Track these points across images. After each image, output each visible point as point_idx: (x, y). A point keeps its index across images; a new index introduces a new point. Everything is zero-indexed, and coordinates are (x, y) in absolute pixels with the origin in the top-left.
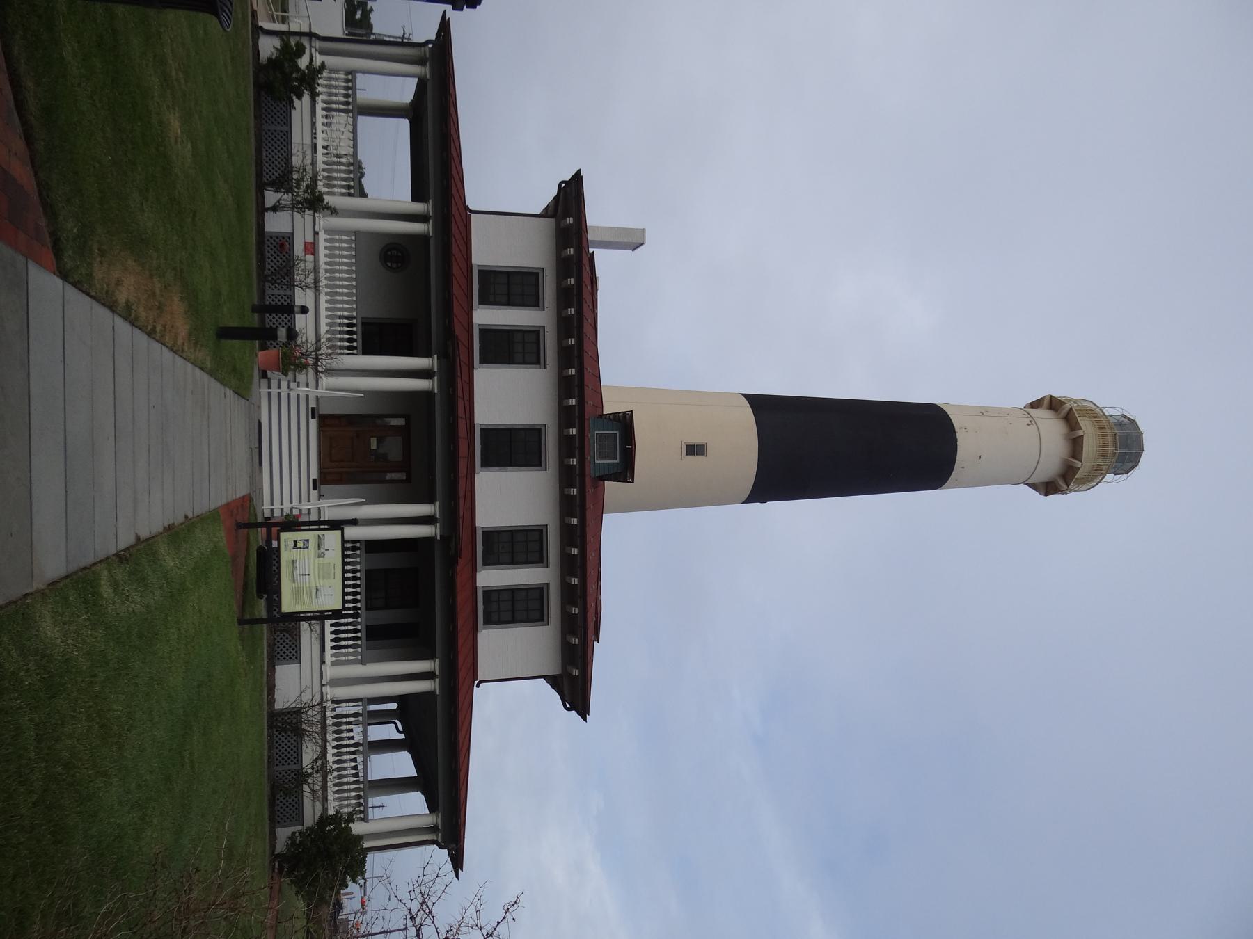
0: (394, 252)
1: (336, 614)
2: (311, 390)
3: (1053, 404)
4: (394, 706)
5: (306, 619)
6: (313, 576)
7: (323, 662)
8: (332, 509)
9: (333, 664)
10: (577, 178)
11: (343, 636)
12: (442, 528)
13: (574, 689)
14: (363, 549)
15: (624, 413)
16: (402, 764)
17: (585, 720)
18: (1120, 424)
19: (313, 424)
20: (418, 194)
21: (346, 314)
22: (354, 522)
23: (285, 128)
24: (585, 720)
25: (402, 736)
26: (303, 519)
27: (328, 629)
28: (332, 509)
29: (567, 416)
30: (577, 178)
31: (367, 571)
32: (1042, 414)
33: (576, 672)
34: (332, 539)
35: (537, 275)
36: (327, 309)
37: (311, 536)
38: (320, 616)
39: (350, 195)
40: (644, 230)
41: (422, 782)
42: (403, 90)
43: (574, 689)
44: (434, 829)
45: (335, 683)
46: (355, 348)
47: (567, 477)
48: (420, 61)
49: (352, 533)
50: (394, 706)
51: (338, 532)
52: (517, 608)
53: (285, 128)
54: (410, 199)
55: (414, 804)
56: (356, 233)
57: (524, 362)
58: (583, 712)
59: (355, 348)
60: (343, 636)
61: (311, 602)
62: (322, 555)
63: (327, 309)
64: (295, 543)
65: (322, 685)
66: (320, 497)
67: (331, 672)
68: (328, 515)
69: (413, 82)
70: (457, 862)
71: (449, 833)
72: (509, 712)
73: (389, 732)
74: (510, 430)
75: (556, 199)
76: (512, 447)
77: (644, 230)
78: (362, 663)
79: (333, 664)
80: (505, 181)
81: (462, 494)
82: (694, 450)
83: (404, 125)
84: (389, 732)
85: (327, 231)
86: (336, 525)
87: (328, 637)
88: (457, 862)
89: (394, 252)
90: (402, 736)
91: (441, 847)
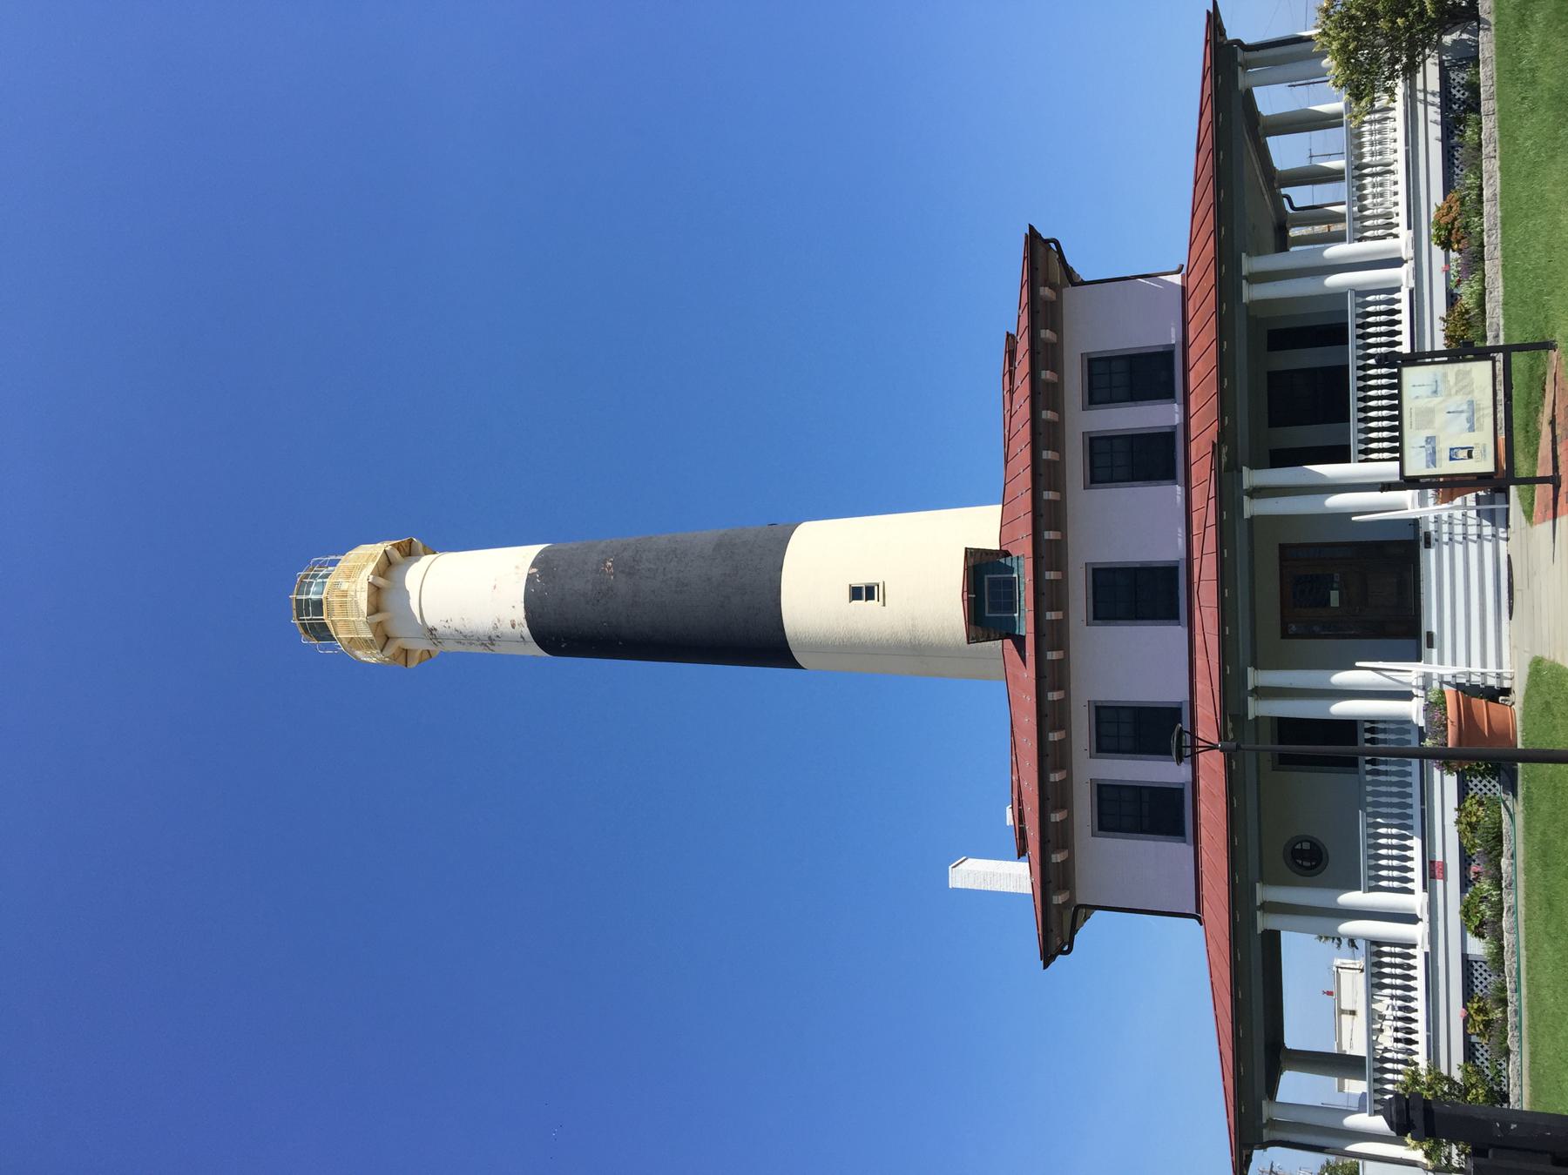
0: (1307, 864)
1: (1415, 359)
2: (1435, 669)
5: (1434, 354)
6: (1448, 411)
8: (1408, 504)
9: (1398, 290)
10: (1048, 958)
13: (1043, 260)
16: (1286, 152)
17: (1031, 227)
18: (718, 546)
20: (1272, 941)
22: (1386, 487)
24: (1031, 227)
25: (1284, 191)
27: (1405, 338)
28: (1408, 504)
29: (1051, 636)
30: (1048, 958)
33: (1045, 292)
34: (1416, 467)
35: (1101, 828)
37: (1446, 467)
38: (1432, 357)
40: (970, 553)
41: (1259, 128)
42: (1295, 1087)
43: (1043, 260)
44: (1247, 65)
46: (1367, 730)
48: (1273, 1124)
49: (1390, 470)
50: (1294, 232)
51: (1408, 473)
54: (1283, 933)
55: (1272, 100)
58: (1033, 237)
59: (1367, 730)
60: (1383, 329)
61: (1445, 375)
64: (1470, 456)
66: (1415, 523)
68: (1408, 496)
69: (1282, 1096)
70: (1214, 22)
71: (1227, 62)
72: (1142, 230)
74: (1137, 618)
75: (1074, 931)
76: (1141, 594)
77: (970, 553)
80: (1158, 969)
81: (1212, 502)
82: (856, 593)
83: (1294, 1038)
84: (1301, 196)
86: (1409, 483)
87: (1404, 327)
88: (1214, 22)
89: (1307, 864)
90: (1284, 191)
91: (1238, 42)
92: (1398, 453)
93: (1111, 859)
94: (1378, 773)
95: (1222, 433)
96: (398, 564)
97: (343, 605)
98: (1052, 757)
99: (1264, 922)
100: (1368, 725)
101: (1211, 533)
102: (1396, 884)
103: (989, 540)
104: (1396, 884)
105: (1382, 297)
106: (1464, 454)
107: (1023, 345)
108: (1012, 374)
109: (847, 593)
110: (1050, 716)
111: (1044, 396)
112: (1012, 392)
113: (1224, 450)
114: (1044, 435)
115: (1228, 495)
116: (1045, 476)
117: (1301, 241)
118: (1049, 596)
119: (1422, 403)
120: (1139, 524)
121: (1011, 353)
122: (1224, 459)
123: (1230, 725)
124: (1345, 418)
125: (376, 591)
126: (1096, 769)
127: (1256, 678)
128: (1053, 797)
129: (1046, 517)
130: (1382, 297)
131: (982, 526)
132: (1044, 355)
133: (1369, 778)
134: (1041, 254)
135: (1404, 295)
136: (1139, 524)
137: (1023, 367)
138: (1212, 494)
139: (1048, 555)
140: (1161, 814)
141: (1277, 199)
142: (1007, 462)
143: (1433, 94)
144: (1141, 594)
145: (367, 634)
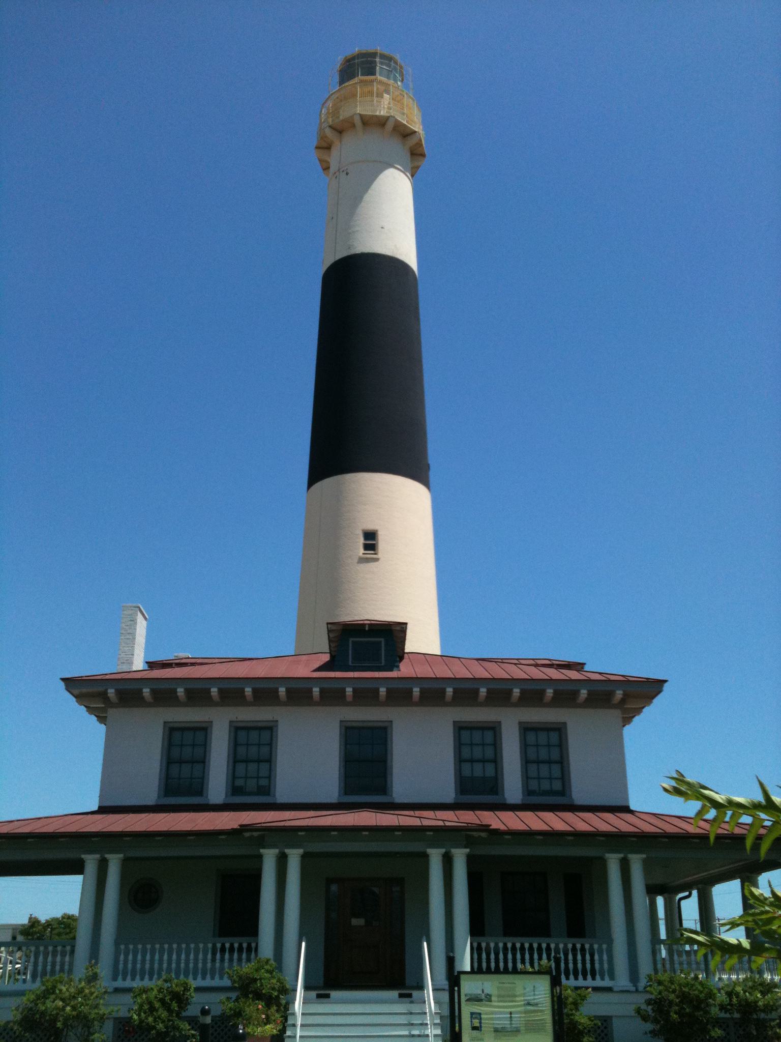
3: (325, 147)
4: (660, 901)
7: (609, 990)
9: (612, 978)
10: (70, 683)
11: (580, 966)
12: (457, 847)
14: (481, 939)
15: (329, 631)
19: (334, 994)
20: (73, 867)
21: (209, 956)
23: (467, 769)
25: (695, 893)
26: (446, 1012)
29: (332, 696)
31: (506, 934)
32: (334, 159)
34: (469, 986)
36: (213, 978)
37: (467, 1010)
39: (72, 952)
45: (634, 976)
46: (249, 946)
47: (400, 695)
50: (660, 901)
51: (462, 977)
52: (548, 753)
53: (467, 769)
56: (117, 943)
57: (271, 744)
59: (249, 946)
62: (489, 998)
63: (213, 978)
64: (474, 1028)
65: (637, 991)
67: (622, 980)
73: (690, 909)
76: (366, 766)
78: (610, 942)
79: (612, 978)
81: (441, 823)
84: (690, 909)
85: (115, 979)
86: (454, 979)
90: (695, 893)
92: (477, 970)
93: (148, 731)
94: (214, 954)
95: (496, 832)
96: (412, 160)
97: (371, 93)
98: (231, 692)
99: (91, 862)
100: (253, 945)
101: (416, 822)
102: (121, 966)
103: (412, 645)
104: (121, 966)
105: (606, 966)
106: (476, 1023)
107: (573, 675)
108: (550, 666)
109: (370, 527)
110: (265, 692)
111: (532, 694)
112: (536, 665)
113: (483, 835)
114: (499, 693)
115: (442, 835)
116: (466, 692)
117: (653, 905)
118: (366, 695)
119: (519, 991)
120: (423, 760)
121: (568, 666)
122: (475, 834)
123: (256, 834)
124: (507, 933)
125: (381, 123)
126: (220, 724)
127: (294, 857)
128: (198, 693)
129: (433, 692)
130: (606, 966)
131: (424, 639)
132: (566, 695)
133: (210, 945)
134: (649, 689)
135: (607, 983)
136: (423, 760)
137: (554, 674)
138: (448, 824)
139: (400, 695)
140: (181, 784)
141: (688, 887)
142: (478, 660)
143: (733, 924)
144: (366, 766)
145: (344, 114)
